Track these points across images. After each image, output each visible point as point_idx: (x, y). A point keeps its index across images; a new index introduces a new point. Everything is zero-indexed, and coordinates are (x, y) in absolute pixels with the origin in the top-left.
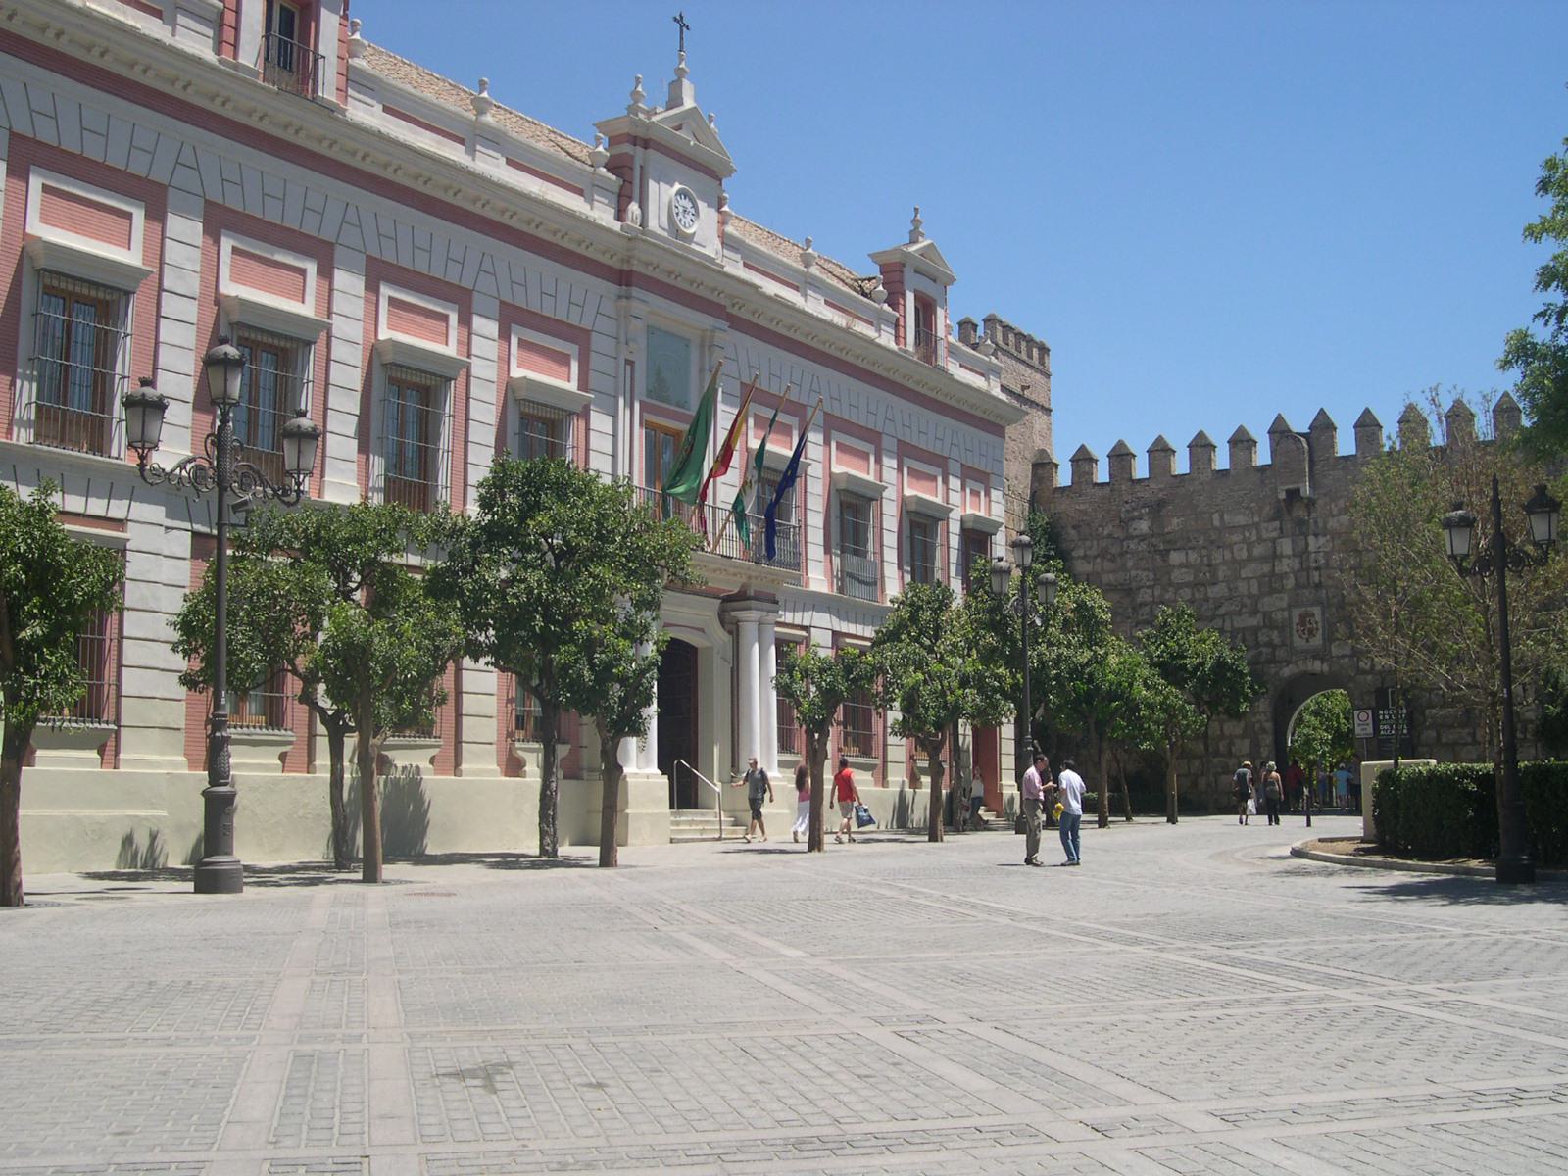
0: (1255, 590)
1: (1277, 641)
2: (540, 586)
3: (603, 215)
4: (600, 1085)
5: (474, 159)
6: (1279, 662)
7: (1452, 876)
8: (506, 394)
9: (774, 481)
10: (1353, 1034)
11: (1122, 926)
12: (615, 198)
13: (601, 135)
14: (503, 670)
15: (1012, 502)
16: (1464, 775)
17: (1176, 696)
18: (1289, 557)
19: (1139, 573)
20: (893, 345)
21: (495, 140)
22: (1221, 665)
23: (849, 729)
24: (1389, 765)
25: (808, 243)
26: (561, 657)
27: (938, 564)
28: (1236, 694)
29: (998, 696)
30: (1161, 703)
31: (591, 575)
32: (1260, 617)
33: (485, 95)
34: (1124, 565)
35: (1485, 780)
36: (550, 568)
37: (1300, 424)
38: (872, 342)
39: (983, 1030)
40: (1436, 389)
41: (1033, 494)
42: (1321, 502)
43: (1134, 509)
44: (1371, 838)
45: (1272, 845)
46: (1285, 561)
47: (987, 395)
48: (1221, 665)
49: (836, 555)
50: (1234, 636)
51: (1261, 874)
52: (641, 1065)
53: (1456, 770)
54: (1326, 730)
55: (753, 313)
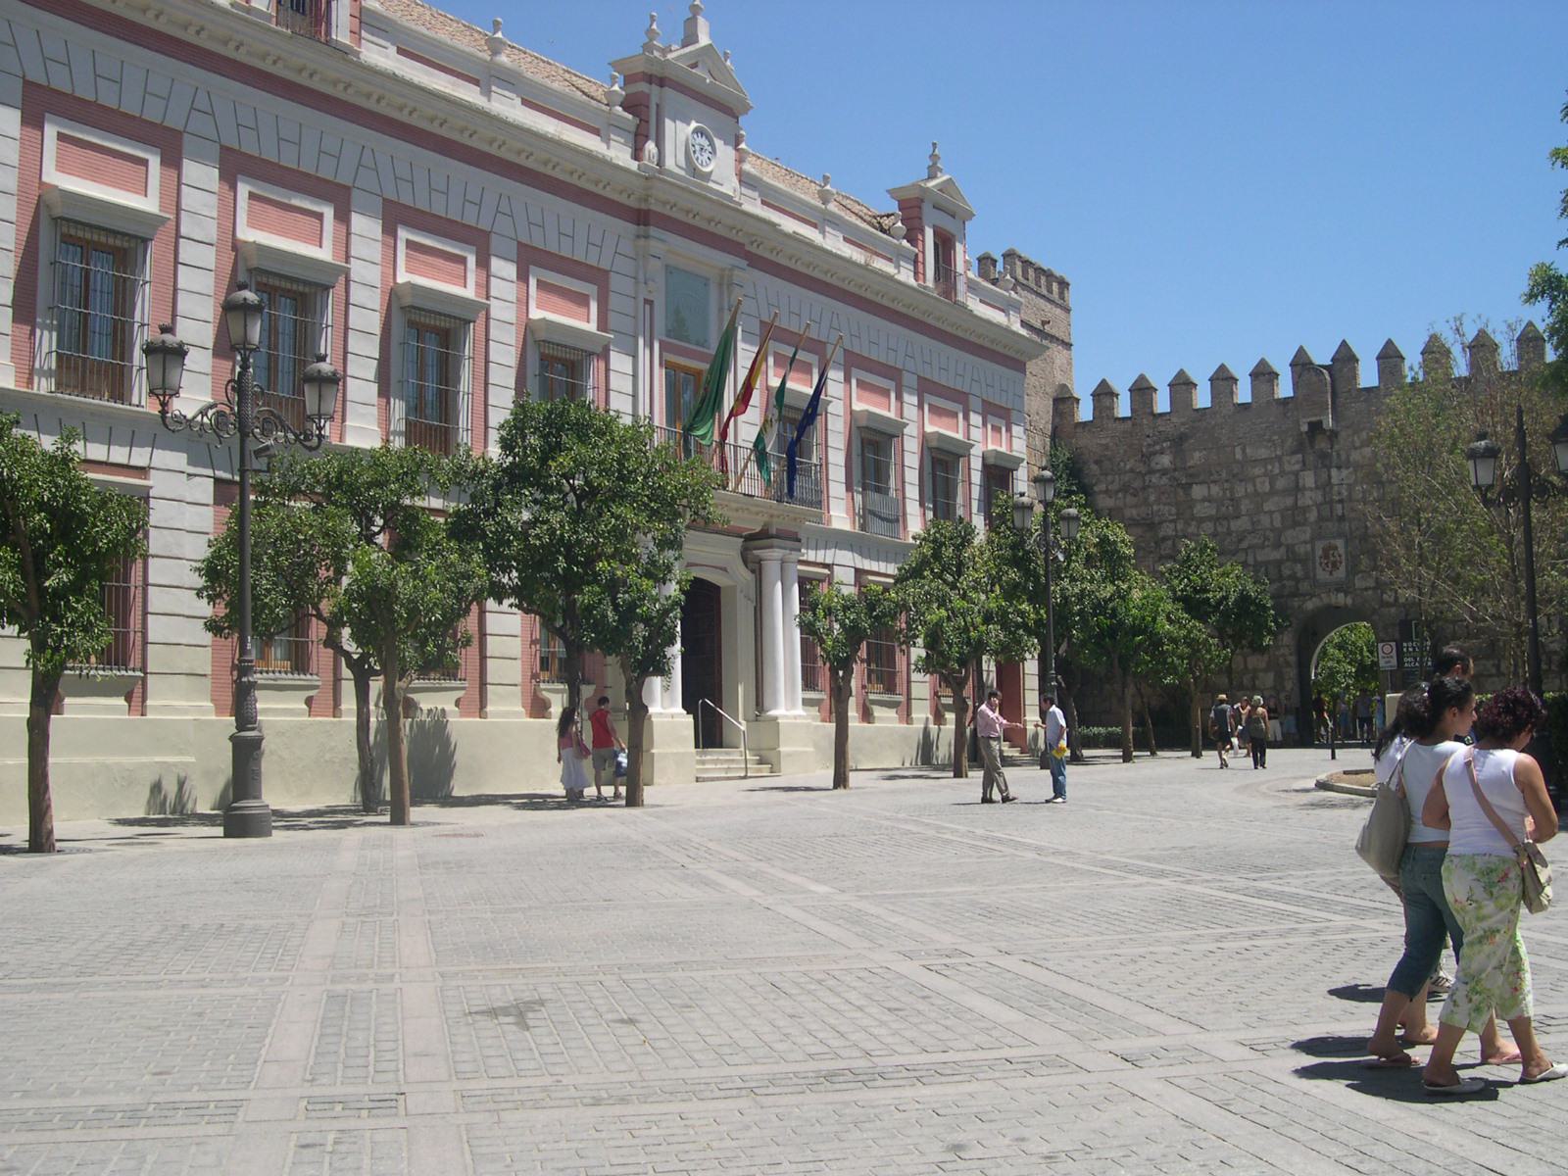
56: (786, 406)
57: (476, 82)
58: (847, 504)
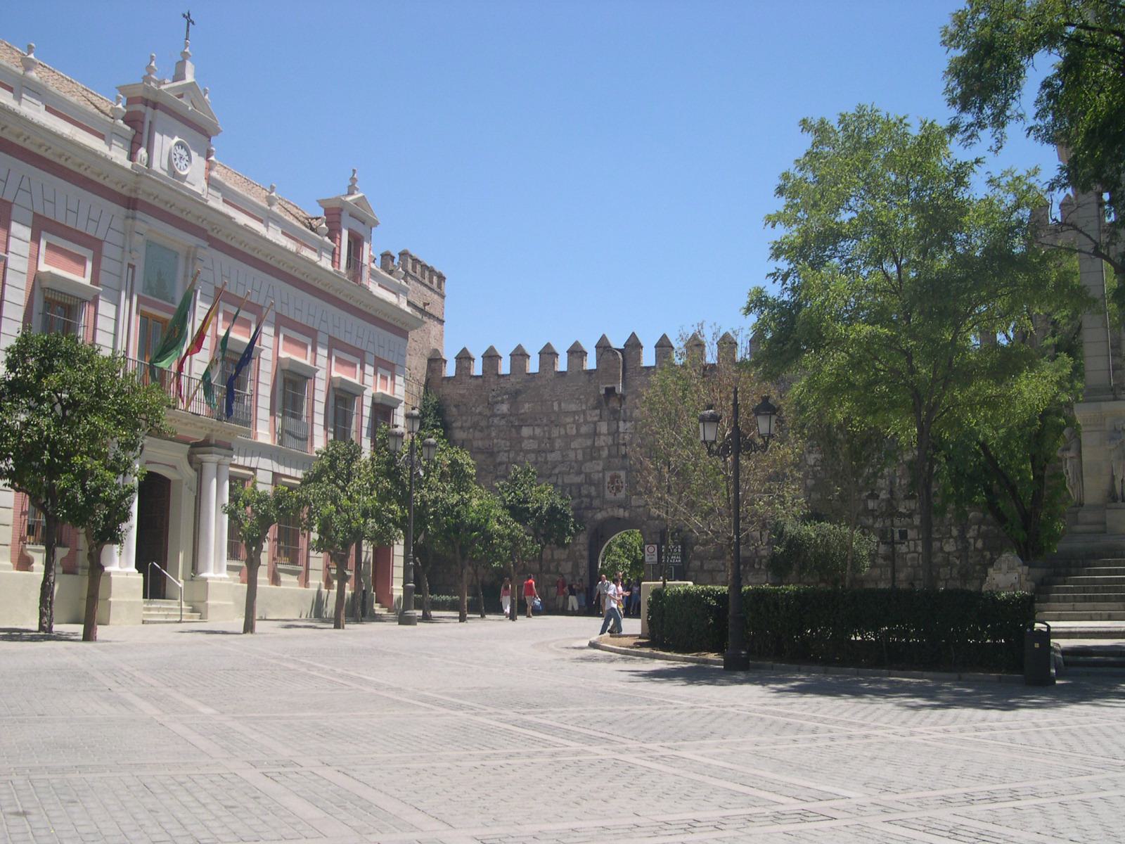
0: (580, 457)
1: (594, 493)
2: (49, 428)
3: (119, 156)
4: (25, 814)
5: (20, 104)
6: (594, 508)
7: (695, 664)
8: (34, 283)
9: (235, 361)
10: (592, 779)
11: (453, 696)
12: (128, 144)
13: (121, 96)
14: (18, 490)
15: (412, 386)
16: (708, 594)
17: (519, 529)
18: (605, 435)
19: (499, 440)
20: (330, 267)
21: (37, 91)
22: (553, 509)
23: (282, 544)
24: (659, 585)
25: (272, 188)
26: (61, 482)
27: (353, 427)
28: (564, 531)
29: (391, 525)
30: (509, 535)
31: (88, 422)
32: (583, 476)
33: (32, 56)
34: (489, 435)
35: (722, 598)
36: (58, 416)
37: (618, 342)
38: (314, 264)
39: (328, 773)
40: (702, 324)
41: (428, 380)
42: (629, 398)
43: (498, 395)
44: (646, 635)
45: (577, 639)
46: (602, 438)
47: (396, 308)
48: (553, 509)
49: (279, 417)
50: (563, 489)
51: (563, 660)
52: (62, 797)
53: (703, 591)
54: (627, 558)
55: (227, 237)
58: (270, 425)
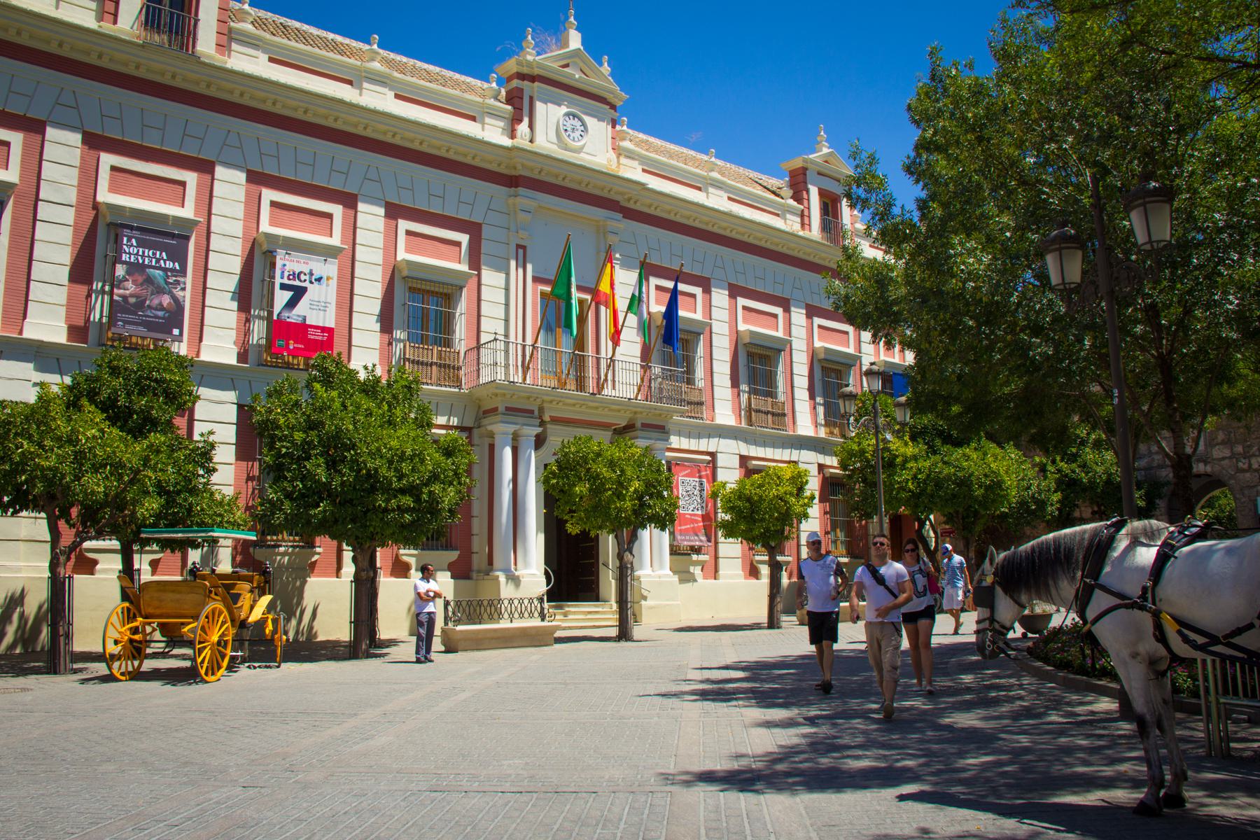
56: (681, 330)
57: (350, 83)
58: (733, 404)
